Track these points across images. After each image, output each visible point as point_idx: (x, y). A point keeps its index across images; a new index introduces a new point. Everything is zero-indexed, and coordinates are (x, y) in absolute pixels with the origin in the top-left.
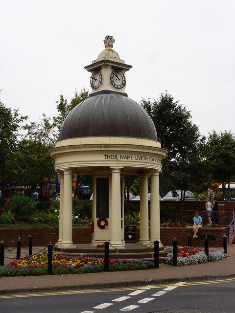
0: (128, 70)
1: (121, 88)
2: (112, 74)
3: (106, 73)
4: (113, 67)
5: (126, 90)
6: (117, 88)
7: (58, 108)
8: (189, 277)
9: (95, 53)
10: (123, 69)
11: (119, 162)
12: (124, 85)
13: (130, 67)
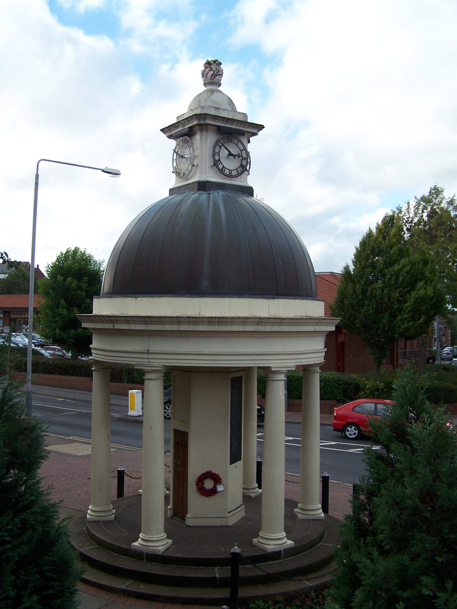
0: (254, 134)
1: (239, 175)
2: (217, 143)
3: (204, 143)
4: (220, 130)
5: (251, 180)
6: (230, 176)
7: (76, 250)
8: (316, 579)
9: (184, 94)
10: (242, 133)
11: (151, 356)
12: (244, 169)
13: (261, 127)
